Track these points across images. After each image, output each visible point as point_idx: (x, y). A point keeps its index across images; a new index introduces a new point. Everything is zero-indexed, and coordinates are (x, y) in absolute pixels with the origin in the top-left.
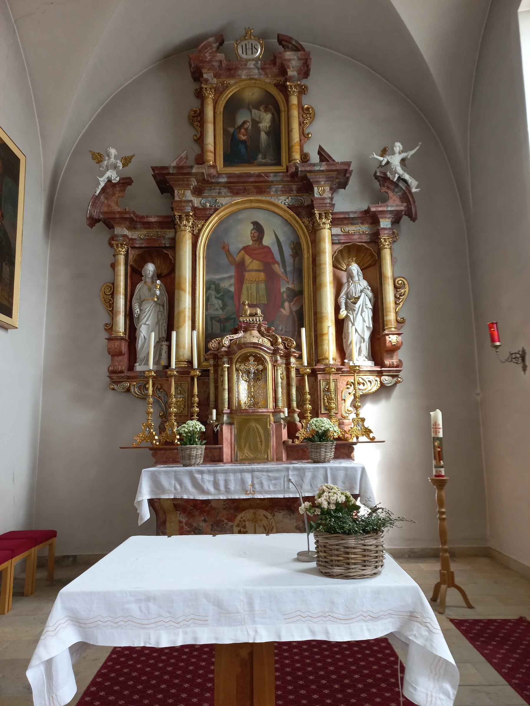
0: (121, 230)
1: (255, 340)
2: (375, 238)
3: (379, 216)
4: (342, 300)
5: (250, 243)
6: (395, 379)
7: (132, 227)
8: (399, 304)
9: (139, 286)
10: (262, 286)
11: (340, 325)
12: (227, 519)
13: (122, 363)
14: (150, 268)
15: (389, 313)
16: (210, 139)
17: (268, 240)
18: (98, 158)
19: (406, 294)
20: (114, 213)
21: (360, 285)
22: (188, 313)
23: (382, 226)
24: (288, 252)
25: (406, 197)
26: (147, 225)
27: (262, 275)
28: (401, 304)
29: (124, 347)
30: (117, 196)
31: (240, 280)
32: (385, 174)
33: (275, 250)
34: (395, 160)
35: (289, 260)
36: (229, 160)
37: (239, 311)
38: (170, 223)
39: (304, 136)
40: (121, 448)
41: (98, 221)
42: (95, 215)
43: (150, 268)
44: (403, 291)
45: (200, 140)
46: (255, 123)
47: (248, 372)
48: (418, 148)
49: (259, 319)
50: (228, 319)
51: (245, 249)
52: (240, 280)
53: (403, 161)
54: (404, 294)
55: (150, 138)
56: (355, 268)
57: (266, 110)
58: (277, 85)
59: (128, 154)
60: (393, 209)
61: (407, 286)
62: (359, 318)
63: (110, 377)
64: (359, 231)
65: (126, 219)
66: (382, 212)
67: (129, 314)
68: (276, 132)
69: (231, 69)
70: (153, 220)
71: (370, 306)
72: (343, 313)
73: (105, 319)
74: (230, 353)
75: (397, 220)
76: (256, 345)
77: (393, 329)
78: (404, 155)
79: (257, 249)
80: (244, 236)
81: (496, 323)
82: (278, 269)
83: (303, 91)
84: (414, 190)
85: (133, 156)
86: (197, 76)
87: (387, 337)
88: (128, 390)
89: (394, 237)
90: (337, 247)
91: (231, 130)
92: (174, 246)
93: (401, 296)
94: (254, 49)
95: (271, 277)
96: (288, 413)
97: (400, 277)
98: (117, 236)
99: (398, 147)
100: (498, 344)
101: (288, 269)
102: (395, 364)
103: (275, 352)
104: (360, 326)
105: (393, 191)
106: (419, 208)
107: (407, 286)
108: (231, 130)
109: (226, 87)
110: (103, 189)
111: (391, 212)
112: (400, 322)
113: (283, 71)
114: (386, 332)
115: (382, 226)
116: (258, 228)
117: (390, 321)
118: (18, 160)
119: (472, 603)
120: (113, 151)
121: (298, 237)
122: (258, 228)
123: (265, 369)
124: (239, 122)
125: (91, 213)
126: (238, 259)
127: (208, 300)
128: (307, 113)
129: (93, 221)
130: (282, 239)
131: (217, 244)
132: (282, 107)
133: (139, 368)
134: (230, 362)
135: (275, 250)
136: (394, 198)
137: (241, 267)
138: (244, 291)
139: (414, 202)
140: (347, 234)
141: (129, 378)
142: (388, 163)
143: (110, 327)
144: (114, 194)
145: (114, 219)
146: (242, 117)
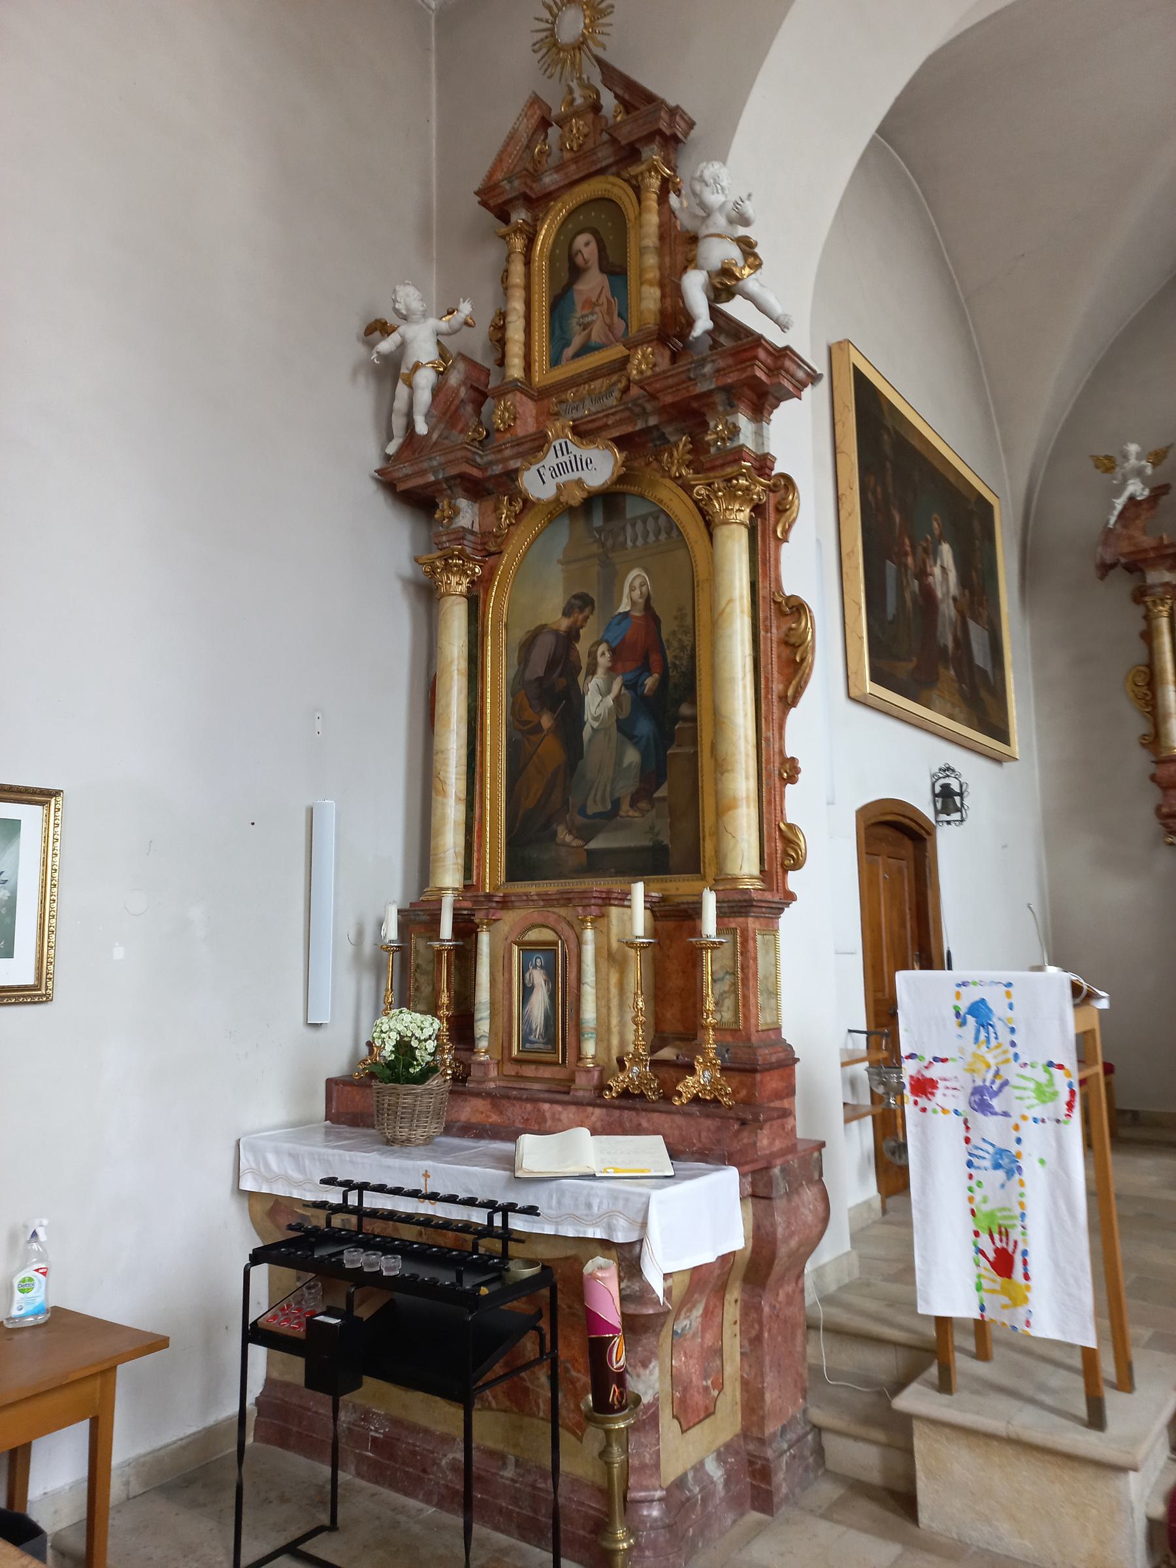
0: (1158, 576)
12: (447, 1122)
18: (1107, 464)
20: (1145, 550)
30: (1143, 517)
40: (310, 812)
41: (1112, 566)
42: (1109, 559)
63: (1164, 825)
65: (1167, 556)
85: (1169, 447)
98: (1153, 587)
110: (1121, 515)
118: (989, 507)
120: (1133, 448)
125: (1102, 558)
144: (1138, 517)
145: (1145, 560)
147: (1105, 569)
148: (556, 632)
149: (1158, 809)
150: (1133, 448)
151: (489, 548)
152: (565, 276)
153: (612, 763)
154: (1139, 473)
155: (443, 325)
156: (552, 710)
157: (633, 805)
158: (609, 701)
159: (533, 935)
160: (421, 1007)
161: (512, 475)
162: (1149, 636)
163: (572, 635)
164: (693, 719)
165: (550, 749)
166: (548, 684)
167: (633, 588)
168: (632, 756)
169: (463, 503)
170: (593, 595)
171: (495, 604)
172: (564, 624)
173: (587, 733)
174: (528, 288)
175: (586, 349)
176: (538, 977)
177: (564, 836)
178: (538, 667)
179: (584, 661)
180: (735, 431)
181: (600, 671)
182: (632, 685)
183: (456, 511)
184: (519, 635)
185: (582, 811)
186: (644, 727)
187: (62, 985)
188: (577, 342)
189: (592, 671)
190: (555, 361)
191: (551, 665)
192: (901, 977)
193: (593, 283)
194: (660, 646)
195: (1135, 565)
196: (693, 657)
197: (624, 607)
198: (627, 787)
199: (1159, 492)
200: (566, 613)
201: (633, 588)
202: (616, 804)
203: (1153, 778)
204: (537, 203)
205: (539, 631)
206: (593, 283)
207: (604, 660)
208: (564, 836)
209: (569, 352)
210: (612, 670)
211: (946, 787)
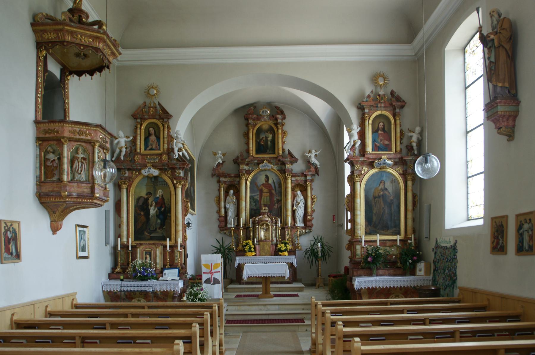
0: (222, 179)
1: (266, 219)
2: (306, 181)
4: (295, 203)
5: (264, 182)
7: (225, 177)
9: (228, 197)
10: (268, 198)
11: (294, 212)
13: (223, 224)
14: (232, 192)
16: (251, 146)
17: (270, 182)
18: (215, 154)
21: (300, 198)
22: (244, 208)
24: (277, 186)
26: (231, 177)
27: (268, 194)
29: (223, 219)
31: (261, 196)
33: (273, 185)
34: (313, 155)
35: (277, 189)
36: (258, 152)
37: (260, 208)
38: (238, 176)
39: (283, 143)
43: (232, 192)
45: (248, 144)
46: (267, 138)
47: (264, 229)
49: (267, 211)
50: (257, 209)
51: (263, 185)
52: (261, 196)
53: (316, 155)
55: (230, 142)
56: (299, 192)
57: (270, 133)
58: (274, 124)
59: (224, 152)
62: (300, 210)
64: (300, 179)
67: (225, 207)
68: (273, 141)
69: (259, 118)
70: (233, 175)
71: (303, 205)
72: (295, 208)
73: (216, 209)
74: (258, 223)
76: (266, 221)
79: (267, 184)
80: (262, 180)
82: (274, 192)
83: (283, 124)
86: (247, 119)
88: (225, 233)
89: (312, 181)
90: (293, 184)
91: (258, 140)
92: (239, 183)
94: (266, 112)
95: (271, 195)
99: (313, 151)
101: (277, 192)
103: (272, 222)
104: (300, 212)
108: (258, 140)
109: (256, 124)
113: (276, 119)
116: (267, 177)
120: (220, 152)
121: (280, 181)
122: (267, 177)
123: (269, 228)
124: (261, 137)
126: (260, 188)
127: (250, 203)
128: (284, 133)
129: (213, 175)
130: (275, 181)
131: (253, 183)
132: (276, 132)
133: (229, 226)
134: (258, 225)
135: (273, 185)
137: (261, 191)
138: (262, 200)
140: (297, 180)
141: (225, 229)
143: (219, 212)
146: (262, 136)
147: (213, 175)
148: (144, 198)
149: (219, 226)
150: (220, 152)
151: (130, 180)
152: (147, 134)
153: (155, 222)
154: (221, 157)
155: (126, 140)
156: (143, 211)
157: (159, 229)
158: (155, 211)
159: (147, 250)
160: (368, 229)
161: (140, 170)
162: (219, 190)
163: (147, 199)
164: (170, 216)
165: (143, 219)
166: (142, 207)
167: (159, 193)
168: (159, 221)
169: (127, 172)
170: (152, 192)
171: (132, 191)
172: (146, 197)
173: (150, 216)
174: (140, 134)
175: (151, 149)
176: (148, 256)
177: (146, 233)
178: (141, 203)
179: (150, 204)
180: (180, 174)
181: (153, 206)
182: (159, 209)
183: (125, 173)
184: (136, 197)
185: (149, 229)
186: (161, 216)
187: (90, 257)
188: (150, 147)
189: (152, 206)
190: (145, 150)
191: (143, 203)
192: (202, 255)
193: (153, 138)
194: (165, 204)
195: (219, 176)
196: (170, 206)
197: (158, 196)
198: (158, 226)
199: (223, 162)
200: (147, 195)
201: (159, 193)
202: (156, 229)
203: (218, 219)
204: (143, 119)
205: (141, 197)
206: (153, 138)
207: (154, 204)
208: (146, 233)
209: (148, 149)
210: (155, 206)
211: (188, 222)
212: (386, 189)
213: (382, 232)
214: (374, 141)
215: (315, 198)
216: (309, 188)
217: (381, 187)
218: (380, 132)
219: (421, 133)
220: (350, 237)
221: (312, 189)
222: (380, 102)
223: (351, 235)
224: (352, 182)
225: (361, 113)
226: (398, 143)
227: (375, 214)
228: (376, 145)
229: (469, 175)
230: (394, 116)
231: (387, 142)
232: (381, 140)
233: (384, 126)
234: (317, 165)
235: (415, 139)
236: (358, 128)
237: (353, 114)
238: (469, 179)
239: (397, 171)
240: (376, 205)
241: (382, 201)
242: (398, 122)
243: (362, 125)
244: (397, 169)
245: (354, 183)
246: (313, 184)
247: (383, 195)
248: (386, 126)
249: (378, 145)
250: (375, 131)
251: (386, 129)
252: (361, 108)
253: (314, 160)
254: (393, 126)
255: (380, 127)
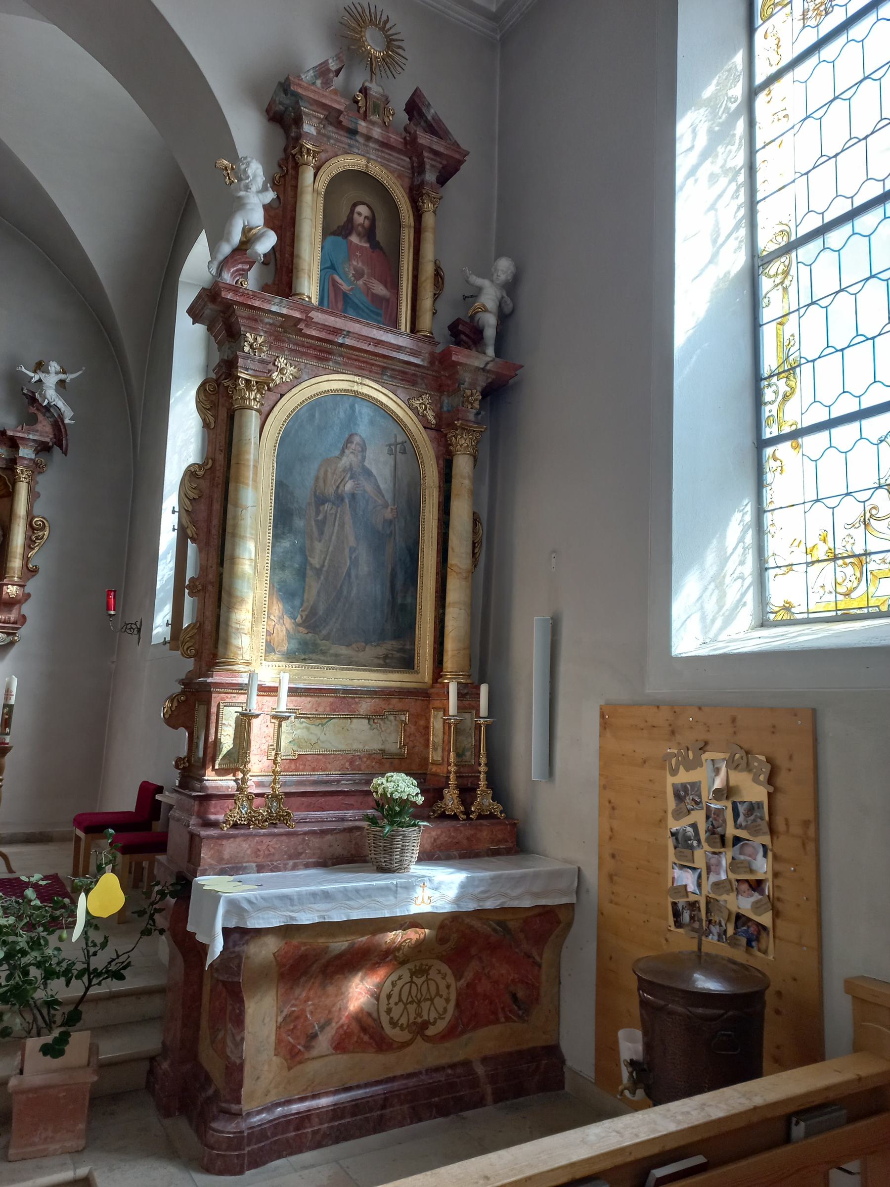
2: (12, 462)
3: (19, 442)
6: (11, 638)
8: (33, 549)
15: (13, 559)
19: (45, 537)
23: (21, 455)
25: (58, 425)
28: (36, 549)
32: (34, 393)
34: (50, 380)
44: (41, 533)
48: (80, 372)
53: (61, 383)
54: (42, 538)
60: (35, 438)
61: (47, 529)
66: (22, 438)
75: (43, 448)
77: (16, 579)
78: (62, 376)
81: (115, 591)
84: (67, 421)
87: (5, 587)
89: (37, 468)
93: (37, 539)
96: (478, 695)
97: (38, 517)
99: (54, 366)
100: (112, 612)
102: (12, 619)
105: (44, 415)
106: (71, 441)
107: (47, 529)
111: (34, 441)
112: (30, 572)
114: (5, 581)
115: (21, 455)
117: (13, 568)
119: (13, 868)
136: (45, 423)
139: (66, 435)
142: (40, 381)
155: (385, 1020)
212: (368, 473)
213: (343, 651)
214: (329, 268)
215: (43, 528)
216: (22, 490)
217: (348, 459)
218: (354, 239)
219: (511, 287)
220: (189, 664)
221: (33, 495)
222: (365, 117)
223: (198, 656)
224: (223, 414)
225: (282, 143)
226: (427, 302)
227: (318, 572)
228: (334, 283)
229: (769, 432)
230: (416, 195)
231: (380, 289)
232: (359, 275)
233: (373, 219)
234: (61, 417)
235: (490, 298)
236: (264, 189)
237: (246, 130)
238: (768, 451)
239: (414, 410)
240: (321, 533)
241: (348, 518)
242: (429, 219)
243: (285, 178)
244: (416, 403)
245: (231, 418)
246: (40, 478)
247: (353, 496)
248: (380, 225)
249: (345, 287)
250: (336, 229)
251: (380, 235)
252: (282, 116)
253: (51, 395)
254: (407, 236)
255: (358, 220)
